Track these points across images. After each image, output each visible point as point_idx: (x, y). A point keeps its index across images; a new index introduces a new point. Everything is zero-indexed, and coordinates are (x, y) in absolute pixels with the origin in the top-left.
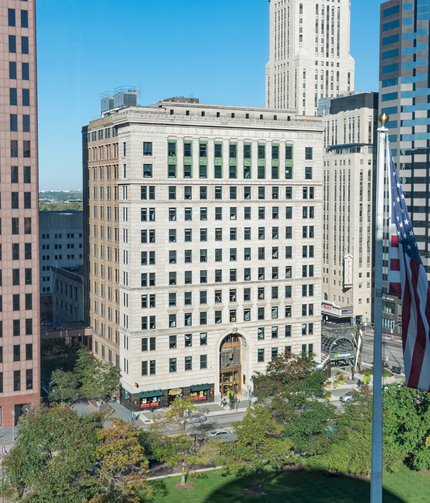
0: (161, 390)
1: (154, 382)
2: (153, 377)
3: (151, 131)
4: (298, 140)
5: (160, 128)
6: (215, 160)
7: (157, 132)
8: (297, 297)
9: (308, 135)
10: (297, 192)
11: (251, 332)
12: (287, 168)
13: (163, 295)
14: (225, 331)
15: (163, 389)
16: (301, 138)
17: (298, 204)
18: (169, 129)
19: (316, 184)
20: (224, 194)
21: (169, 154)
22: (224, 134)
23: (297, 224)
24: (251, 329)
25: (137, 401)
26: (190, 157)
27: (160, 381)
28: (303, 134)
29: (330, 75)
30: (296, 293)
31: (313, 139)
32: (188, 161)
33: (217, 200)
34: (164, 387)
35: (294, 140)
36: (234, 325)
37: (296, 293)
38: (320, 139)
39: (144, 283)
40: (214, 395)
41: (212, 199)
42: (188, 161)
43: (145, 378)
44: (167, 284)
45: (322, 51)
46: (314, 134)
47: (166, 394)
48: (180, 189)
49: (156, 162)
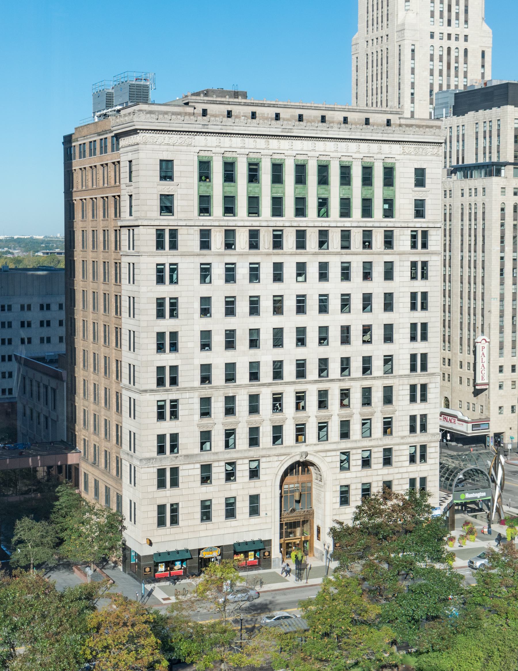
0: (187, 551)
1: (177, 537)
2: (175, 529)
3: (171, 142)
4: (402, 156)
5: (185, 137)
6: (272, 188)
7: (181, 145)
8: (401, 403)
9: (419, 148)
10: (402, 238)
11: (329, 459)
12: (386, 201)
13: (191, 401)
14: (288, 457)
15: (190, 548)
16: (408, 154)
17: (404, 257)
18: (200, 140)
19: (431, 225)
20: (287, 241)
21: (200, 179)
22: (287, 147)
23: (402, 289)
24: (329, 454)
25: (150, 568)
26: (232, 184)
27: (186, 536)
28: (413, 146)
29: (453, 54)
30: (400, 398)
31: (426, 155)
32: (230, 189)
33: (276, 251)
34: (192, 546)
35: (397, 157)
36: (303, 448)
37: (400, 398)
38: (438, 155)
39: (160, 382)
40: (270, 558)
41: (268, 249)
42: (230, 189)
43: (162, 531)
44: (197, 382)
45: (441, 17)
46: (428, 147)
47: (195, 557)
48: (218, 234)
49: (180, 191)
